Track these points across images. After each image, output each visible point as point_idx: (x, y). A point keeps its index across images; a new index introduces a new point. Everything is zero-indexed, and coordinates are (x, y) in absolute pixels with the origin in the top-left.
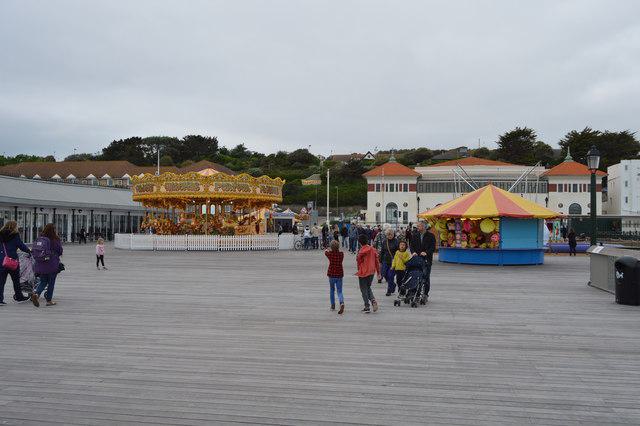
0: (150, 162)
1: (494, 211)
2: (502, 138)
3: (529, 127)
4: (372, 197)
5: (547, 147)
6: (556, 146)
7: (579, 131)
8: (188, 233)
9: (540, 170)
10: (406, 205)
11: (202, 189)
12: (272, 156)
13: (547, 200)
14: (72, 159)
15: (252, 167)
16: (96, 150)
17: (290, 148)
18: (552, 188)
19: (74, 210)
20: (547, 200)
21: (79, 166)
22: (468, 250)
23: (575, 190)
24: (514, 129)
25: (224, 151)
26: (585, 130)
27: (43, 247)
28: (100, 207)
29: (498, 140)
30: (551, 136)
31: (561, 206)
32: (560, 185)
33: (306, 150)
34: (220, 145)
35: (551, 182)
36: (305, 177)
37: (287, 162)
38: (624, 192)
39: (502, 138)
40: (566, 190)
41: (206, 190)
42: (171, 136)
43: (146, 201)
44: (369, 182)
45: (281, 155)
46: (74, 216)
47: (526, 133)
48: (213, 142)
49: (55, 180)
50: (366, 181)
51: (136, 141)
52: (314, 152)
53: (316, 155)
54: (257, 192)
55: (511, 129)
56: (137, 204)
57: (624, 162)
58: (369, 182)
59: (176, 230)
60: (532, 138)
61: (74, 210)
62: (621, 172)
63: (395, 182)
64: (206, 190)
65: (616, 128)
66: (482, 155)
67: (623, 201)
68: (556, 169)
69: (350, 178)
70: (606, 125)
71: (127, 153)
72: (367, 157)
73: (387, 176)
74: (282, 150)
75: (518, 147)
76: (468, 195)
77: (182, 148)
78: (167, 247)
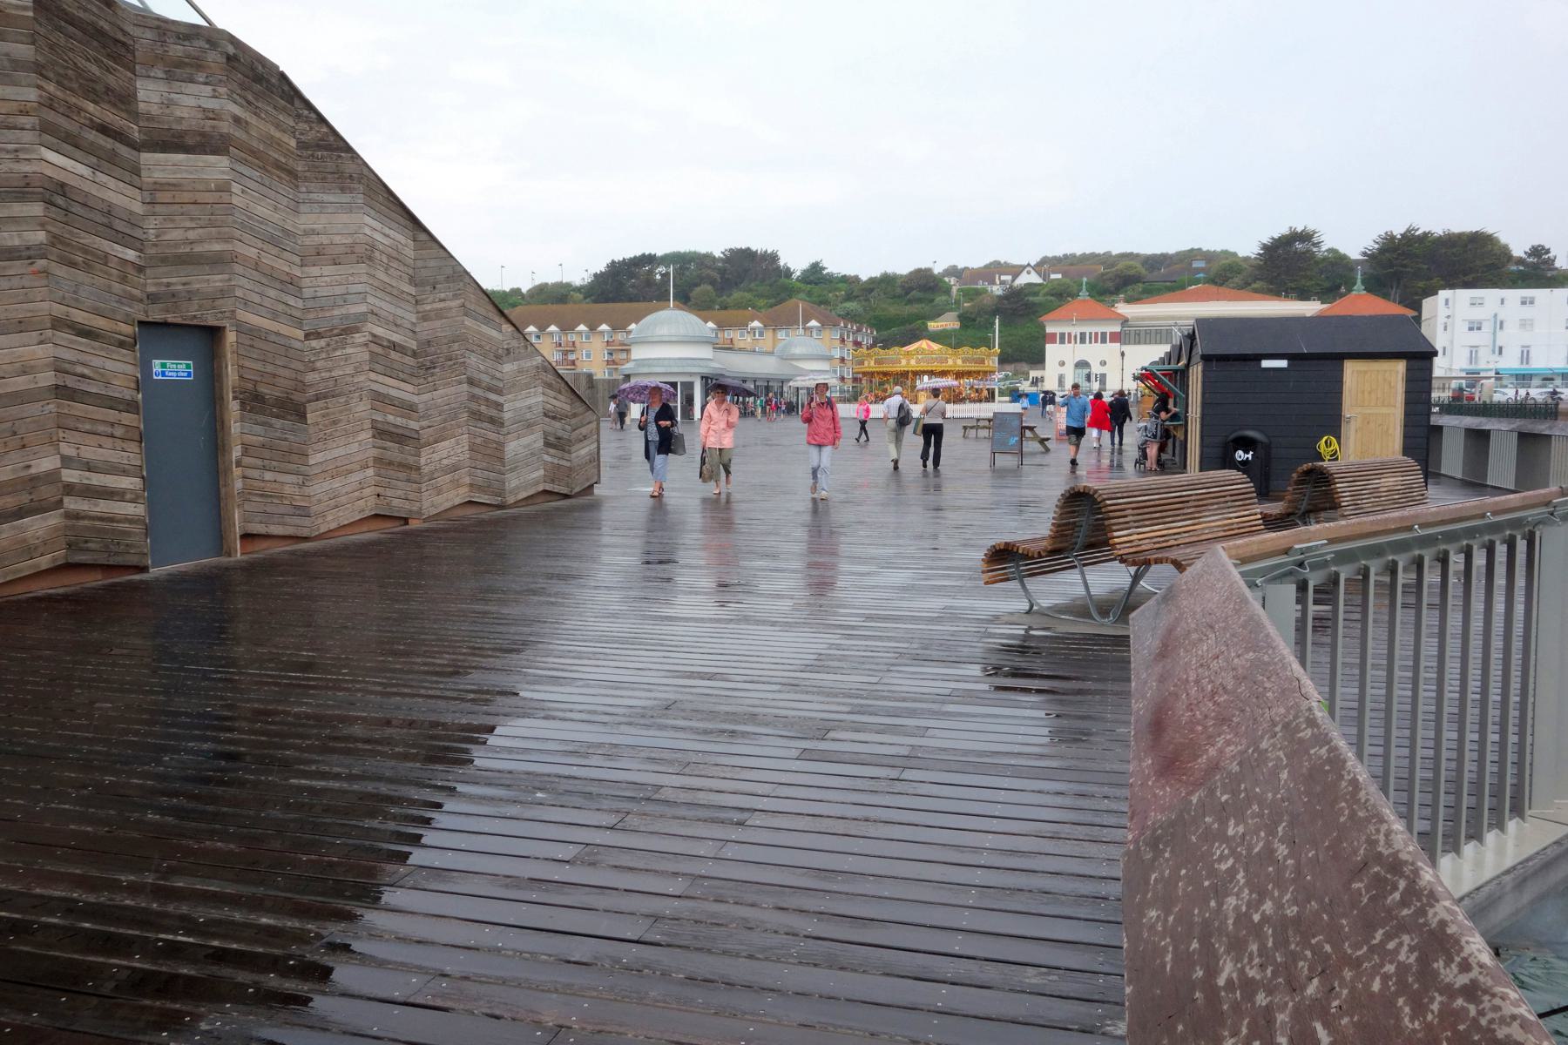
3: (1311, 227)
7: (1398, 231)
26: (1408, 231)
37: (899, 291)
47: (1305, 236)
50: (1043, 328)
55: (1280, 230)
57: (1444, 294)
60: (1317, 245)
77: (722, 272)
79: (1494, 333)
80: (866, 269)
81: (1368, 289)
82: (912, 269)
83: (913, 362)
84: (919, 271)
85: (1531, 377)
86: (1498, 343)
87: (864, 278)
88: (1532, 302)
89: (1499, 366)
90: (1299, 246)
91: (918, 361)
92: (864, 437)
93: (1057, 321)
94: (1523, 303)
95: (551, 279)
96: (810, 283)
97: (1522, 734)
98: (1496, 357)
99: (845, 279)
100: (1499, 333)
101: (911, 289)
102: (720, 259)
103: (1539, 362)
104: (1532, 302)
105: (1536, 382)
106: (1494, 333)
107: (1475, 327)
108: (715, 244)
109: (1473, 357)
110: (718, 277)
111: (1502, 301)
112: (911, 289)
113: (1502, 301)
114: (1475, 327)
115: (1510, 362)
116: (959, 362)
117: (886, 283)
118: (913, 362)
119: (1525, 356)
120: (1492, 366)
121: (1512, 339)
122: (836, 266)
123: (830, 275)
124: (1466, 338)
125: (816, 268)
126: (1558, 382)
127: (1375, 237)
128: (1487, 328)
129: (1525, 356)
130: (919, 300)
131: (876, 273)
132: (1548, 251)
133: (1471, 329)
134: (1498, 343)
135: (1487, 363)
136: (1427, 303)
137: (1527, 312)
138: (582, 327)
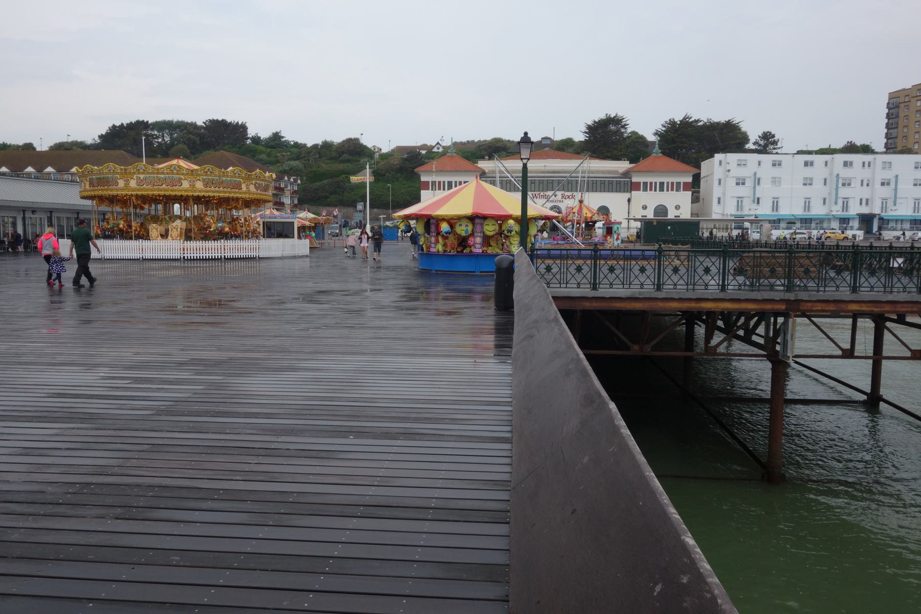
0: (165, 153)
1: (468, 210)
2: (589, 127)
3: (620, 114)
4: (424, 194)
5: (642, 137)
6: (651, 138)
7: (678, 118)
8: (247, 237)
9: (623, 166)
10: (678, 207)
11: (121, 183)
12: (315, 146)
13: (629, 200)
14: (60, 148)
15: (289, 160)
16: (90, 134)
17: (337, 138)
18: (635, 187)
19: (24, 211)
20: (629, 200)
21: (66, 156)
22: (444, 255)
23: (662, 189)
24: (603, 116)
25: (256, 140)
26: (685, 118)
27: (904, 263)
28: (66, 207)
29: (584, 129)
30: (646, 124)
31: (645, 207)
32: (645, 184)
33: (357, 140)
34: (251, 133)
35: (635, 179)
36: (355, 173)
37: (334, 154)
38: (717, 192)
39: (589, 127)
40: (651, 190)
41: (127, 185)
42: (188, 119)
43: (101, 199)
44: (423, 179)
45: (327, 145)
46: (24, 219)
47: (616, 121)
48: (242, 129)
49: (29, 175)
50: (419, 177)
51: (141, 126)
52: (368, 141)
53: (370, 145)
54: (248, 190)
55: (600, 115)
56: (88, 202)
57: (718, 157)
58: (423, 179)
59: (206, 235)
60: (624, 126)
61: (24, 211)
62: (720, 168)
63: (666, 180)
64: (127, 185)
65: (720, 117)
66: (565, 148)
67: (715, 201)
68: (643, 163)
69: (405, 171)
70: (708, 111)
71: (127, 140)
72: (435, 150)
73: (441, 171)
74: (329, 139)
75: (606, 138)
76: (447, 193)
77: (201, 137)
78: (236, 254)
79: (754, 188)
80: (310, 139)
81: (663, 153)
82: (344, 138)
83: (133, 183)
84: (349, 141)
85: (779, 221)
86: (757, 196)
87: (309, 145)
88: (780, 165)
89: (758, 212)
90: (612, 128)
91: (140, 182)
92: (84, 280)
93: (430, 172)
94: (774, 165)
95: (64, 139)
96: (272, 147)
97: (558, 172)
98: (755, 206)
99: (296, 145)
100: (757, 188)
101: (343, 153)
102: (202, 127)
103: (785, 211)
104: (780, 165)
105: (783, 225)
106: (754, 188)
107: (741, 182)
108: (199, 117)
109: (739, 206)
110: (197, 140)
111: (759, 164)
112: (343, 153)
113: (759, 164)
114: (741, 182)
115: (764, 210)
116: (199, 185)
117: (326, 148)
118: (133, 183)
119: (775, 206)
120: (752, 213)
121: (766, 191)
122: (291, 136)
123: (287, 142)
124: (734, 191)
125: (276, 136)
126: (798, 225)
127: (663, 122)
128: (749, 183)
129: (775, 206)
130: (348, 161)
131: (319, 141)
132: (773, 136)
133: (738, 184)
134: (757, 196)
135: (750, 210)
136: (705, 165)
137: (776, 172)
138: (30, 169)
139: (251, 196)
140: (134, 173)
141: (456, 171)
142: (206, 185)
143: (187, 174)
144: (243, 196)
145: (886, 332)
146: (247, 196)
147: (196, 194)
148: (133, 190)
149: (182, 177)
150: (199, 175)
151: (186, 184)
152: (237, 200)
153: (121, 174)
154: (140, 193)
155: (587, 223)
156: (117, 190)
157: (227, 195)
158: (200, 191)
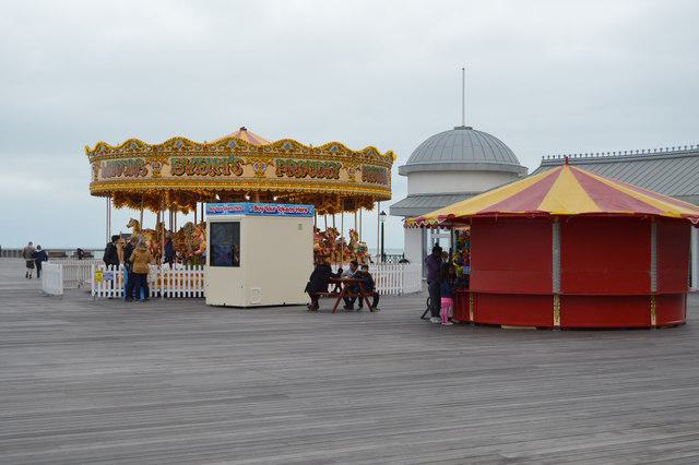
64: (156, 174)
116: (270, 172)
139: (356, 190)
140: (169, 154)
141: (573, 329)
142: (280, 173)
143: (252, 155)
144: (342, 189)
145: (336, 300)
146: (350, 190)
147: (265, 187)
148: (166, 182)
149: (244, 159)
150: (269, 155)
151: (249, 171)
152: (333, 197)
153: (252, 155)
154: (175, 187)
155: (132, 297)
156: (338, 185)
157: (316, 189)
158: (272, 184)
